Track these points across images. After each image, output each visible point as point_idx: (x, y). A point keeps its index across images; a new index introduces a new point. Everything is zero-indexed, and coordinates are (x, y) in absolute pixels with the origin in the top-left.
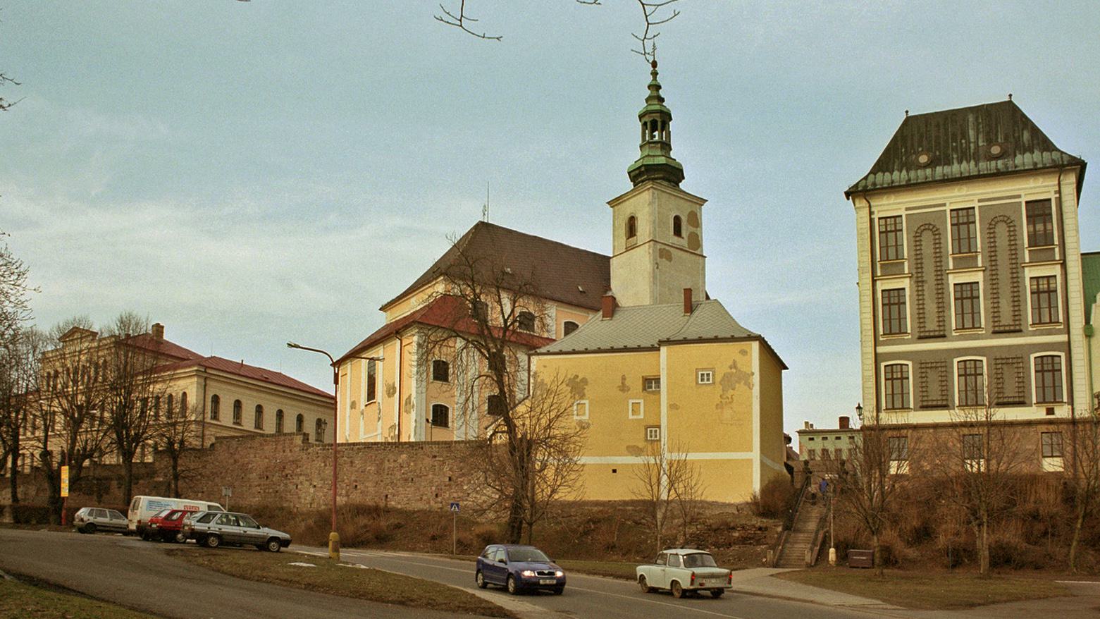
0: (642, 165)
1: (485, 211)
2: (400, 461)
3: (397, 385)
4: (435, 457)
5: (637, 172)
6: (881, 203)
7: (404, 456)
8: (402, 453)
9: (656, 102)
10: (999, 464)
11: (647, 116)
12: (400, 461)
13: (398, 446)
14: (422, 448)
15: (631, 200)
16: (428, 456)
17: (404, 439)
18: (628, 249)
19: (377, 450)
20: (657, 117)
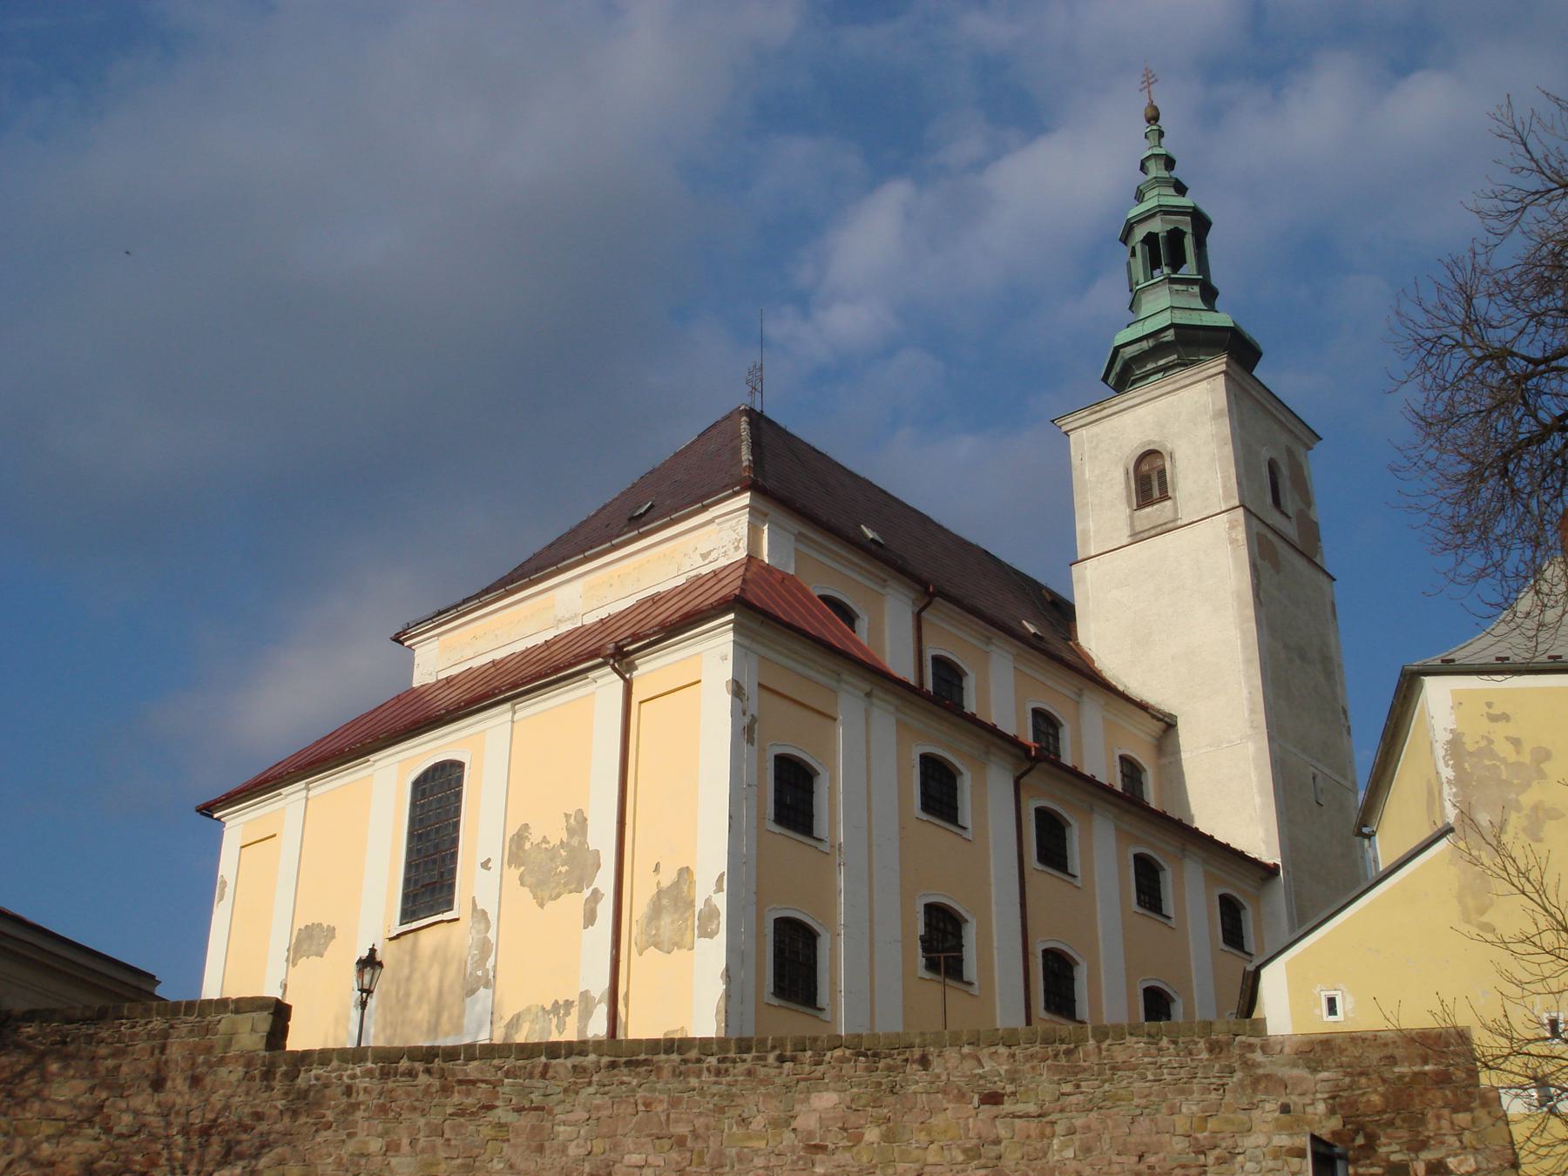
0: (1172, 326)
1: (756, 382)
2: (807, 1121)
3: (602, 838)
4: (993, 1098)
5: (1151, 343)
6: (1049, 683)
7: (827, 1099)
8: (816, 1084)
9: (1172, 191)
10: (22, 1074)
11: (1158, 219)
12: (807, 1121)
13: (624, 1058)
14: (924, 1062)
15: (1141, 410)
16: (961, 1097)
17: (641, 1025)
18: (1137, 537)
19: (677, 1073)
20: (1185, 224)
